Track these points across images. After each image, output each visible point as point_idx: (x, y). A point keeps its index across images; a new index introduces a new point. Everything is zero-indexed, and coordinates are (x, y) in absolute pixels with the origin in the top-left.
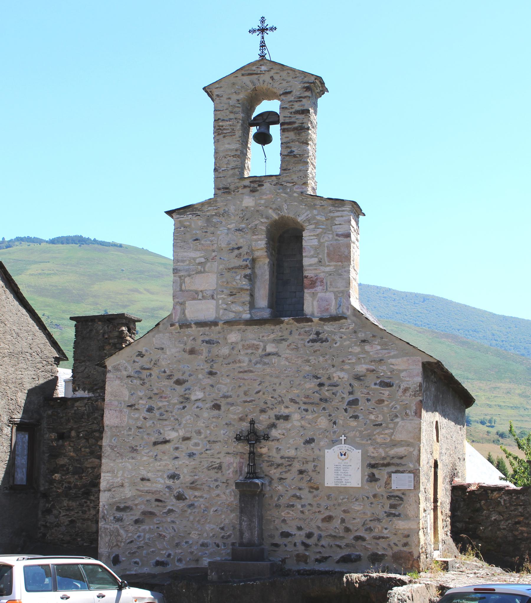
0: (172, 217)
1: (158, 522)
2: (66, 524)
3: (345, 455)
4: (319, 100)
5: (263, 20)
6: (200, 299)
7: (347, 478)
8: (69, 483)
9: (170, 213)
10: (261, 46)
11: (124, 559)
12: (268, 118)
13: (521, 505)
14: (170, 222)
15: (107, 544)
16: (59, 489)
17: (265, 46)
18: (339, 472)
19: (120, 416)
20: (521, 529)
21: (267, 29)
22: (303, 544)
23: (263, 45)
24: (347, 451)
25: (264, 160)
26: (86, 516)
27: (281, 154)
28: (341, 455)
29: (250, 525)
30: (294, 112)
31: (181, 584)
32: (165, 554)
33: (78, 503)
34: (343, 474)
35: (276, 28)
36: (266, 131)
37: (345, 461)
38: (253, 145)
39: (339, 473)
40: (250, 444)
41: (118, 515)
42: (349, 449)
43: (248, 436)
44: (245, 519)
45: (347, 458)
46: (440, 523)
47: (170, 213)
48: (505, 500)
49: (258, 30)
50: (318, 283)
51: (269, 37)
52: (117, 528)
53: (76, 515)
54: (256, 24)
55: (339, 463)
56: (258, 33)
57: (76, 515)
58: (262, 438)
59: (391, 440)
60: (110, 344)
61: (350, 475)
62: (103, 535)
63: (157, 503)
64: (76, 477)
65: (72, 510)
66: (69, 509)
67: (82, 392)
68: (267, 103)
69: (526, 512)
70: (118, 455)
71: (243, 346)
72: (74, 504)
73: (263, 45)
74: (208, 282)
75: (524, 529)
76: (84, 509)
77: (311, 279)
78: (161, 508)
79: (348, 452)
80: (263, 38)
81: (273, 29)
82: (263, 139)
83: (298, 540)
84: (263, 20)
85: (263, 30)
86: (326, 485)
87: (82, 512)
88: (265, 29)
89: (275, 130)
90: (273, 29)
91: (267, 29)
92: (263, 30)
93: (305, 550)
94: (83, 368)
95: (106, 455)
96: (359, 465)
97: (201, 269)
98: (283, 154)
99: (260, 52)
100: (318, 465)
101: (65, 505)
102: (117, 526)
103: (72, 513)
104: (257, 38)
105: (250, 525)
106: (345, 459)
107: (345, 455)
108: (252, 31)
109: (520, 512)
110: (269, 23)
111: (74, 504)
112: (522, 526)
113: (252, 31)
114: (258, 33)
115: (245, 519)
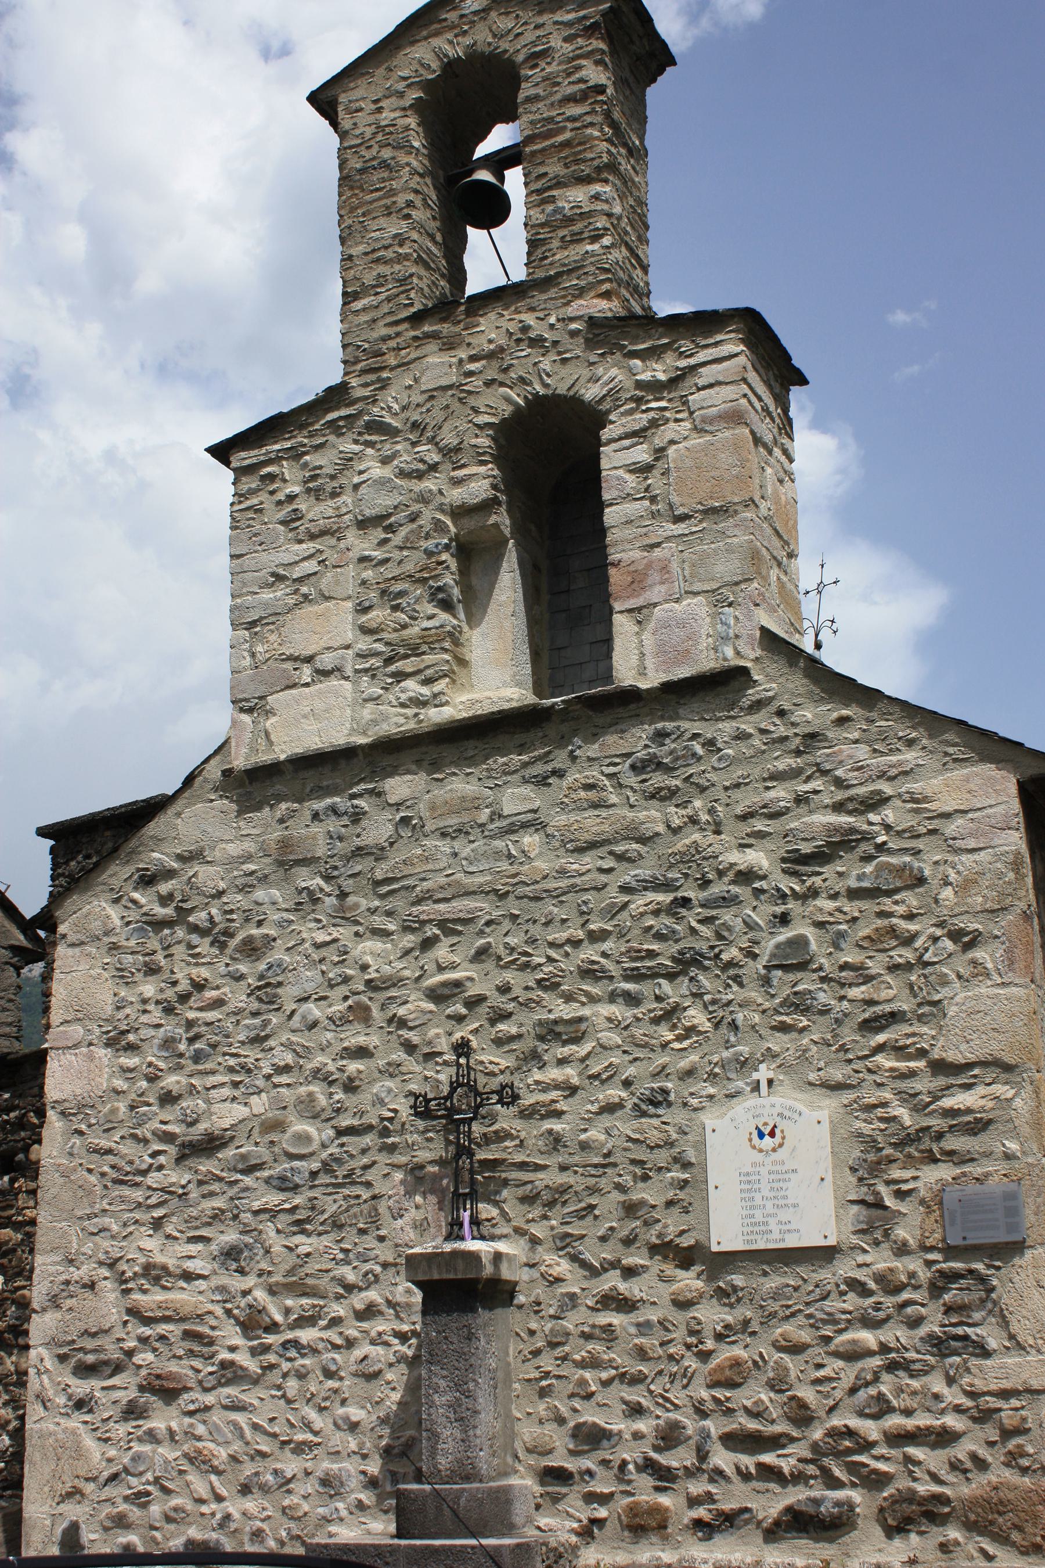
0: (227, 463)
1: (192, 1407)
3: (772, 1134)
4: (653, 93)
6: (307, 685)
7: (784, 1215)
9: (221, 452)
11: (93, 1537)
15: (46, 1489)
18: (758, 1197)
22: (649, 1466)
24: (778, 1119)
27: (526, 225)
28: (761, 1135)
30: (560, 101)
32: (213, 1514)
34: (769, 1205)
37: (774, 1156)
39: (758, 1201)
41: (81, 1387)
42: (787, 1113)
43: (450, 1096)
45: (781, 1145)
46: (711, 341)
47: (221, 452)
50: (655, 576)
52: (74, 1432)
55: (754, 1164)
58: (495, 1098)
59: (687, 974)
61: (795, 1206)
62: (37, 1457)
63: (188, 1345)
70: (80, 1193)
71: (433, 808)
74: (331, 629)
77: (632, 568)
78: (197, 1363)
79: (782, 1125)
83: (631, 1453)
86: (715, 1248)
93: (658, 1489)
95: (48, 1196)
96: (825, 1166)
97: (304, 592)
98: (534, 221)
100: (690, 1174)
102: (75, 1422)
106: (774, 1150)
107: (772, 1134)
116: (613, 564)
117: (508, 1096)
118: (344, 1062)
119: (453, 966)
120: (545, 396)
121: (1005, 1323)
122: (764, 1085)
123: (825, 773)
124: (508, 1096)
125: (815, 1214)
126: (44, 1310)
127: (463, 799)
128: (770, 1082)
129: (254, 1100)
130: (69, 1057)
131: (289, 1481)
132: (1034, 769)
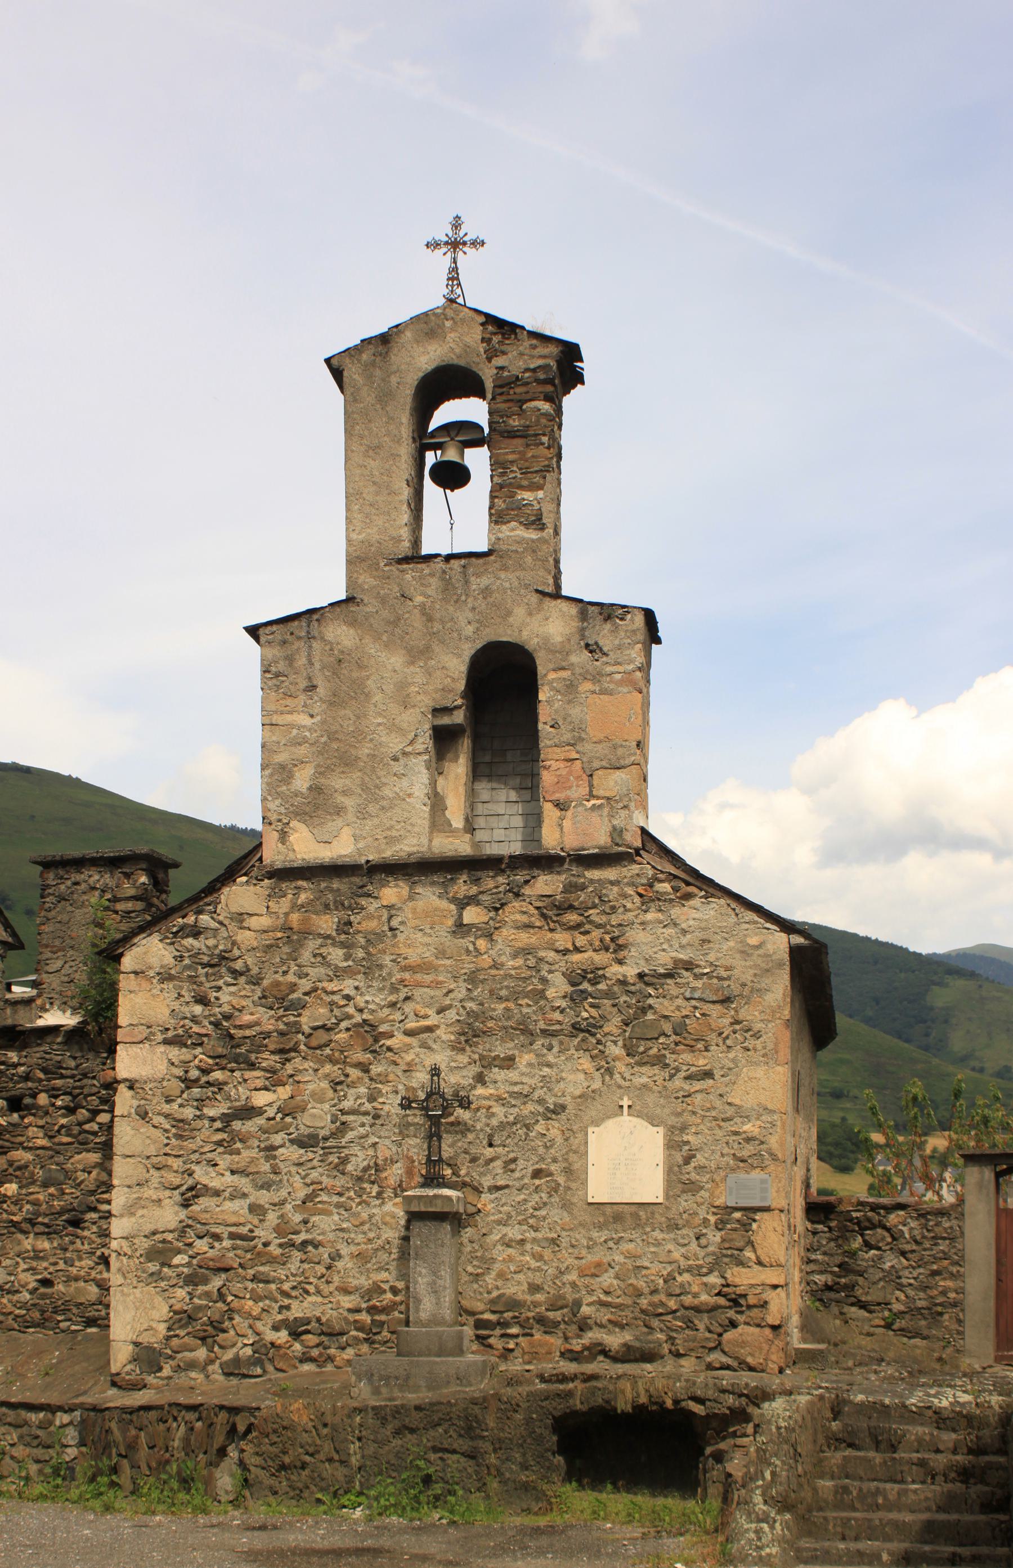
2: (30, 1286)
5: (457, 223)
8: (36, 1203)
9: (253, 631)
10: (449, 279)
12: (466, 434)
13: (944, 1239)
14: (253, 650)
16: (14, 1214)
17: (458, 279)
19: (152, 1060)
20: (942, 1283)
21: (464, 244)
23: (454, 277)
25: (458, 521)
26: (74, 1270)
29: (434, 1283)
31: (296, 1405)
33: (55, 1244)
35: (483, 243)
36: (459, 460)
38: (431, 489)
40: (430, 1117)
44: (424, 1271)
47: (253, 631)
48: (911, 1229)
49: (446, 243)
51: (467, 259)
53: (52, 1269)
54: (442, 232)
56: (445, 250)
57: (52, 1269)
60: (116, 912)
62: (120, 1308)
64: (52, 1190)
65: (42, 1259)
66: (38, 1255)
67: (60, 1013)
68: (472, 395)
69: (953, 1250)
70: (148, 1141)
72: (45, 1244)
73: (454, 277)
75: (949, 1283)
76: (68, 1255)
80: (455, 262)
81: (478, 243)
82: (452, 476)
84: (457, 223)
85: (455, 244)
87: (65, 1263)
88: (459, 243)
89: (477, 460)
90: (478, 243)
91: (464, 244)
92: (455, 244)
94: (59, 964)
99: (446, 291)
101: (29, 1247)
103: (45, 1264)
104: (442, 260)
105: (434, 1283)
108: (433, 245)
109: (943, 1252)
110: (470, 230)
111: (46, 1245)
112: (945, 1279)
113: (433, 245)
114: (445, 250)
115: (424, 1271)
116: (545, 767)
117: (465, 1103)
118: (529, 1298)
119: (426, 1017)
120: (701, 1451)
121: (755, 1251)
122: (625, 1109)
123: (675, 925)
124: (465, 1103)
125: (651, 1188)
126: (122, 1216)
127: (436, 909)
128: (629, 1107)
129: (280, 1089)
130: (135, 1049)
131: (408, 1377)
132: (798, 940)
